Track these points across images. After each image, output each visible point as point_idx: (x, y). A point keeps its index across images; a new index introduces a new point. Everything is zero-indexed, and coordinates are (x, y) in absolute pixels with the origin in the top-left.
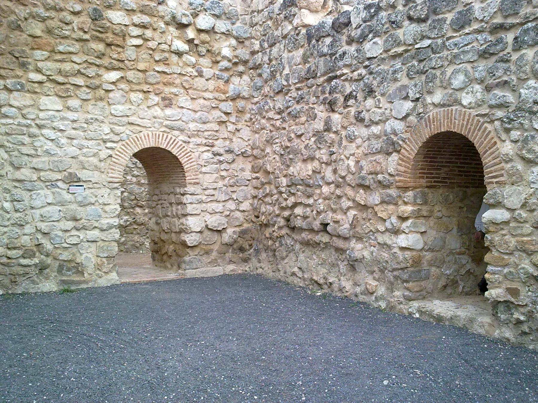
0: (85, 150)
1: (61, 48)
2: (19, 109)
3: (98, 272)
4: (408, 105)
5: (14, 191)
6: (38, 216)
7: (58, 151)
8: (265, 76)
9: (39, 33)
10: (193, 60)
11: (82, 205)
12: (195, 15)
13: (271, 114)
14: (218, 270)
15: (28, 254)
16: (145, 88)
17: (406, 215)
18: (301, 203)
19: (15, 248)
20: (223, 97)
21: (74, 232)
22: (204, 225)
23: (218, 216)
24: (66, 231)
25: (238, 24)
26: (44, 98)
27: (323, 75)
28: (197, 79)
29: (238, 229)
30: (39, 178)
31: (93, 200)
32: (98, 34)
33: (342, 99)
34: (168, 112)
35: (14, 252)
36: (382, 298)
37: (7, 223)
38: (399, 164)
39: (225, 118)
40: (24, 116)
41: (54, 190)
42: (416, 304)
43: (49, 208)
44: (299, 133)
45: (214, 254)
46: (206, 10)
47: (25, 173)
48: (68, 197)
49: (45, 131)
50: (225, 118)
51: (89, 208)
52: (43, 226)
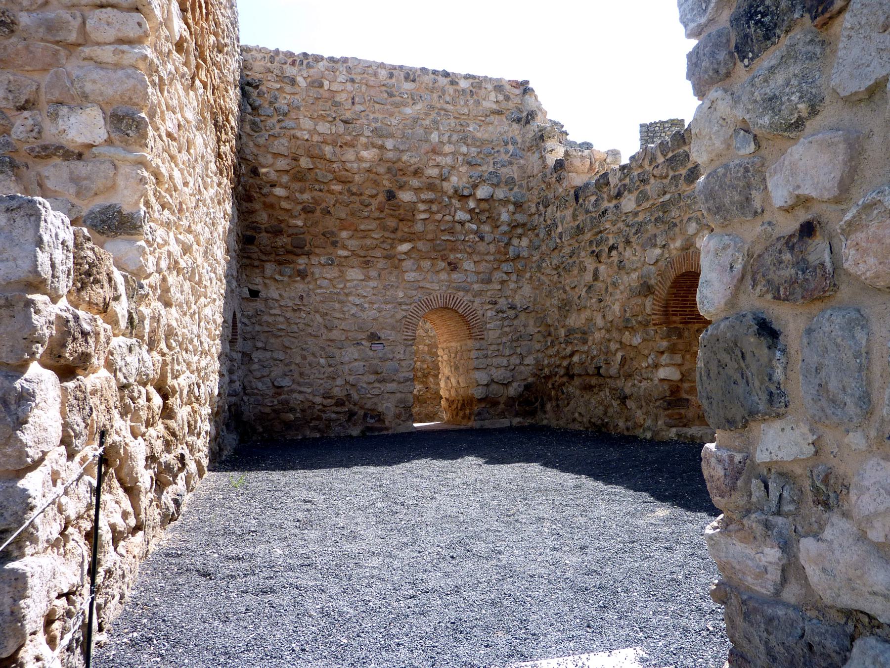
0: (383, 313)
1: (362, 227)
2: (330, 280)
3: (397, 420)
4: (658, 251)
5: (328, 349)
6: (347, 370)
7: (361, 314)
8: (541, 236)
9: (343, 216)
10: (474, 227)
11: (383, 360)
12: (475, 186)
13: (548, 271)
14: (505, 423)
15: (340, 403)
16: (433, 255)
17: (662, 349)
18: (577, 351)
19: (329, 398)
20: (503, 258)
21: (377, 385)
22: (489, 379)
23: (503, 370)
24: (369, 383)
25: (516, 189)
26: (350, 270)
27: (590, 230)
28: (479, 244)
29: (523, 383)
30: (347, 338)
31: (391, 356)
32: (392, 212)
33: (607, 250)
34: (455, 276)
35: (329, 400)
36: (649, 428)
37: (322, 376)
38: (654, 304)
39: (505, 277)
40: (334, 287)
41: (359, 347)
42: (674, 430)
43: (356, 364)
44: (573, 285)
45: (502, 406)
46: (484, 181)
47: (335, 334)
48: (371, 353)
49: (350, 298)
50: (505, 277)
51: (388, 363)
52: (351, 379)
